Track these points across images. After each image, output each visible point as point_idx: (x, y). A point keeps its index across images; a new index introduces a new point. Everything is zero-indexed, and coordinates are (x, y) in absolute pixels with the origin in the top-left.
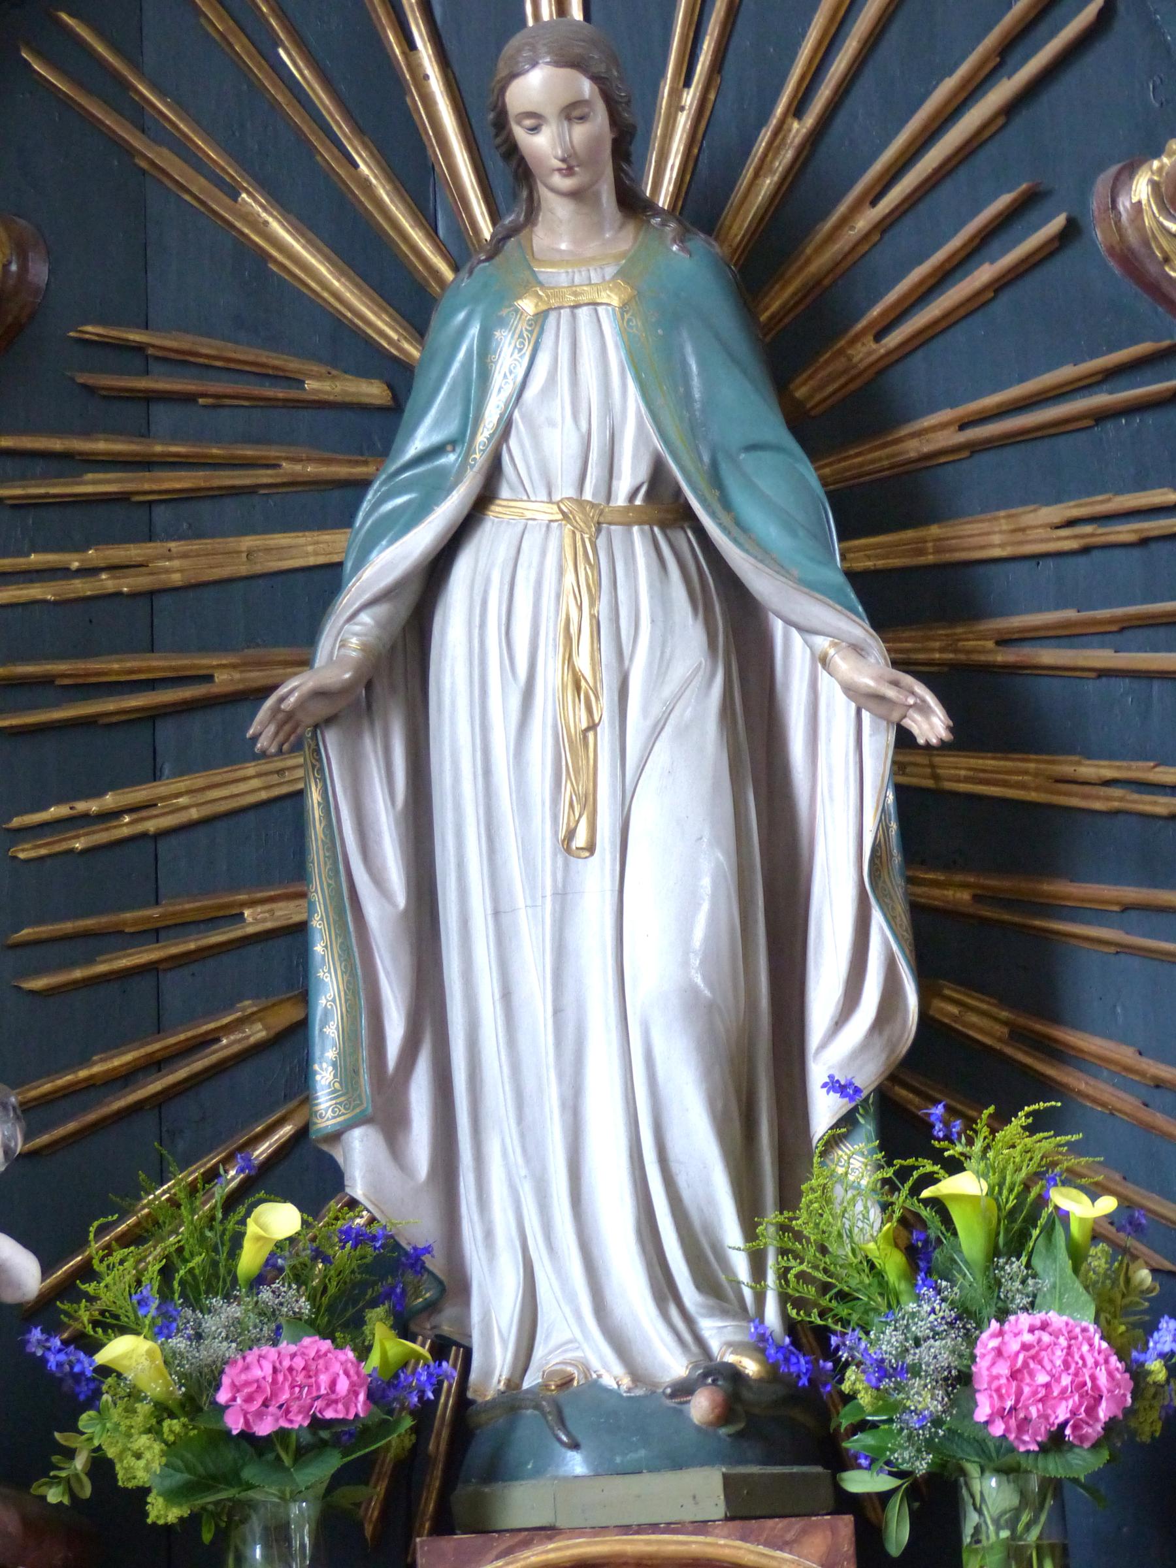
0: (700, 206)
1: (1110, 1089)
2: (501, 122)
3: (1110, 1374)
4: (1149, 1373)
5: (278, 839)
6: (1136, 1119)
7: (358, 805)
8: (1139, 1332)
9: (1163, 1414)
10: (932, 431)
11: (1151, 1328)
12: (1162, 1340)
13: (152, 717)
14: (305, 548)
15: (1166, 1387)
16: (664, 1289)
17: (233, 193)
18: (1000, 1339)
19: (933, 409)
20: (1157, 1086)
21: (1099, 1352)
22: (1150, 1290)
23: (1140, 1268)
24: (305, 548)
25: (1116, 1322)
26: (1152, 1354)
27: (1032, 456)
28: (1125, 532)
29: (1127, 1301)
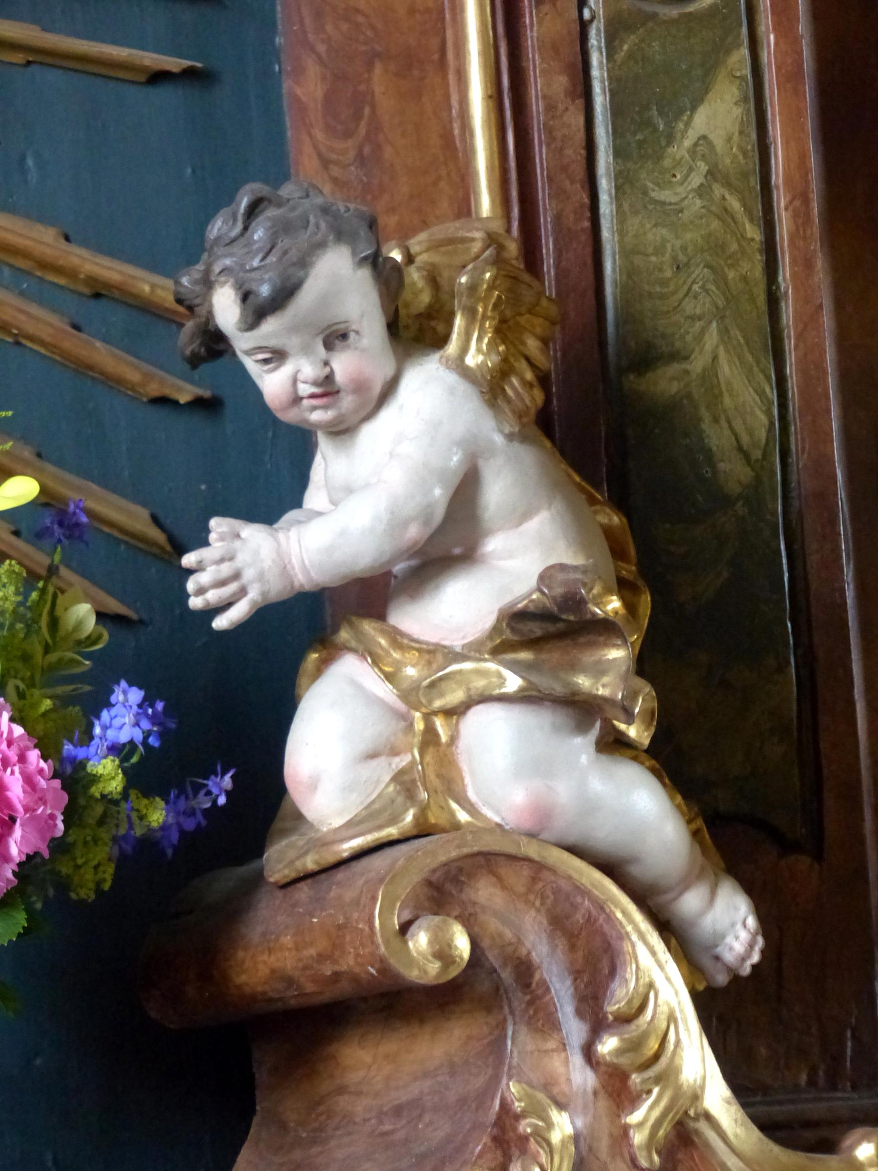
1: (17, 302)
3: (28, 780)
4: (95, 779)
6: (63, 353)
8: (75, 710)
9: (116, 852)
11: (99, 702)
12: (117, 722)
15: (124, 805)
20: (97, 296)
21: (10, 744)
22: (92, 640)
23: (78, 601)
25: (36, 692)
26: (97, 746)
29: (53, 657)
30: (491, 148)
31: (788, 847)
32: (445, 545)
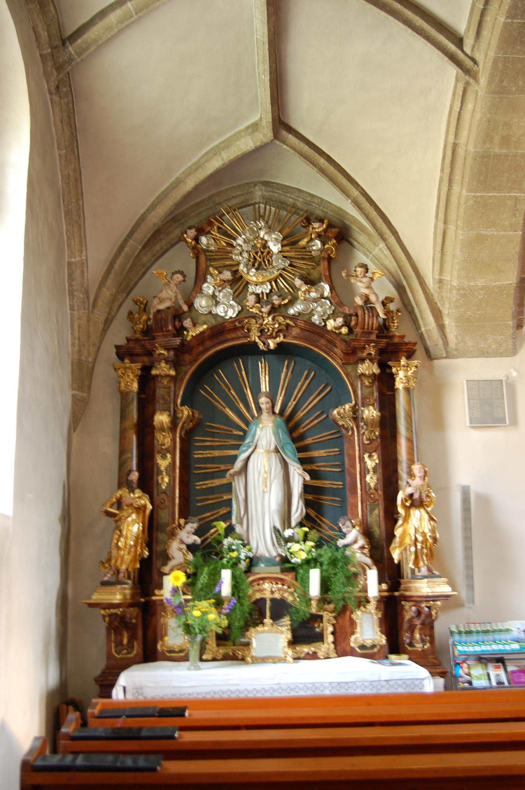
0: (282, 413)
2: (258, 403)
5: (228, 488)
7: (238, 485)
10: (309, 441)
13: (213, 472)
14: (232, 452)
16: (274, 545)
17: (225, 408)
18: (318, 563)
19: (309, 437)
24: (232, 452)
27: (321, 445)
28: (332, 454)
30: (171, 702)
31: (380, 562)
32: (355, 542)
